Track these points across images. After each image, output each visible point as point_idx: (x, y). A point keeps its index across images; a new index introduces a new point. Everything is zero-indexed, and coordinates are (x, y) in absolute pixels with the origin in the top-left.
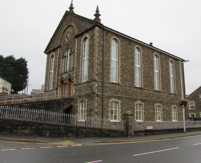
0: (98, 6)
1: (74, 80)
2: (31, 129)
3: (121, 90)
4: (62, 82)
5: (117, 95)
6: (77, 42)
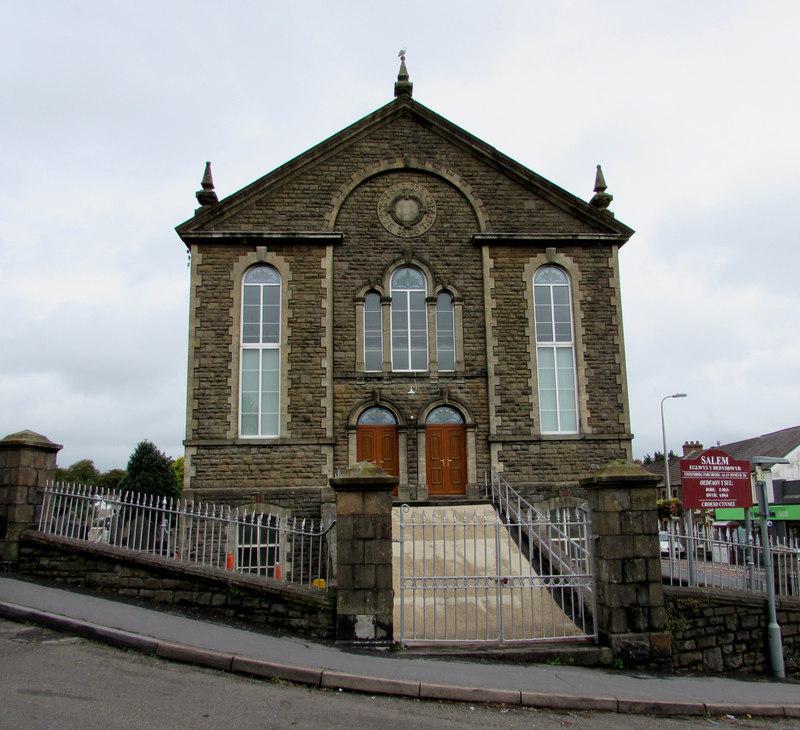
0: (599, 167)
1: (495, 421)
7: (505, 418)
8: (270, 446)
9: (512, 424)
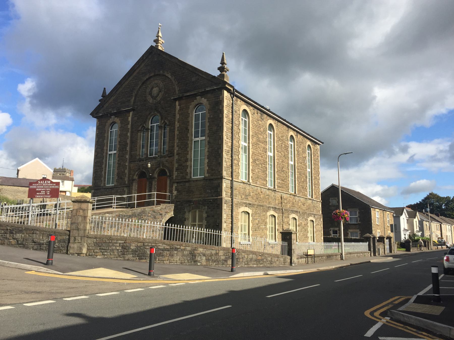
0: (105, 89)
1: (175, 174)
2: (183, 255)
3: (252, 194)
4: (142, 175)
5: (247, 202)
6: (178, 107)
7: (179, 172)
8: (110, 188)
9: (181, 174)
